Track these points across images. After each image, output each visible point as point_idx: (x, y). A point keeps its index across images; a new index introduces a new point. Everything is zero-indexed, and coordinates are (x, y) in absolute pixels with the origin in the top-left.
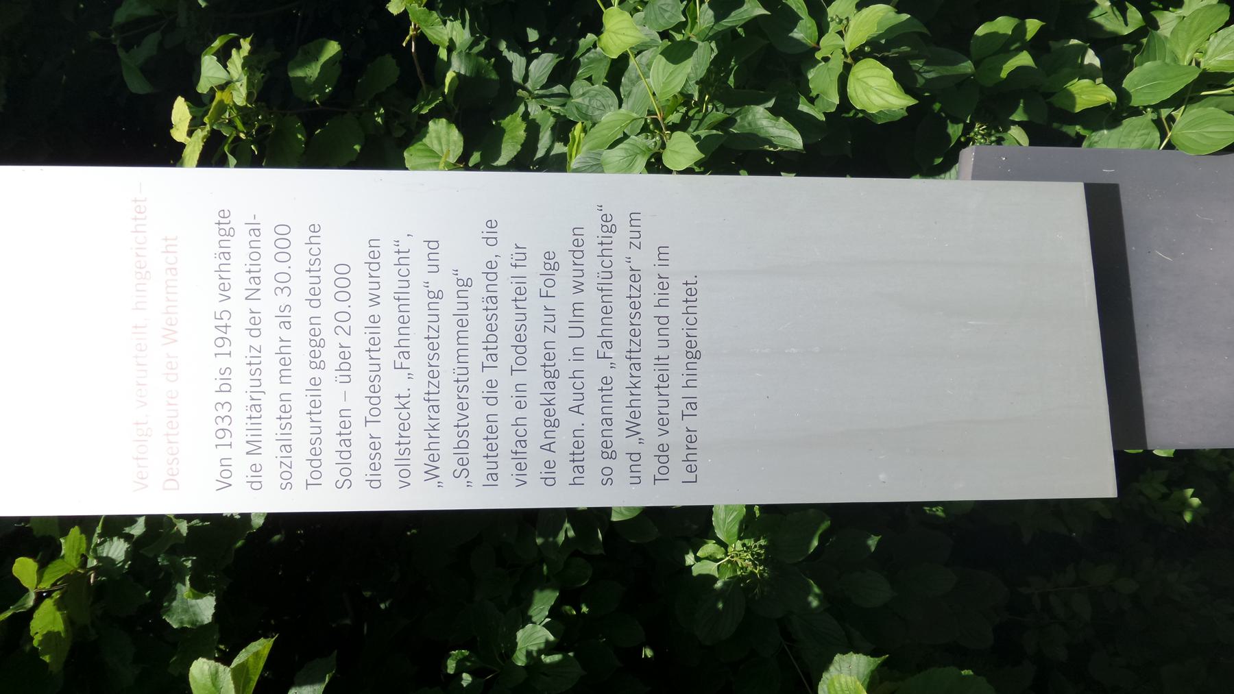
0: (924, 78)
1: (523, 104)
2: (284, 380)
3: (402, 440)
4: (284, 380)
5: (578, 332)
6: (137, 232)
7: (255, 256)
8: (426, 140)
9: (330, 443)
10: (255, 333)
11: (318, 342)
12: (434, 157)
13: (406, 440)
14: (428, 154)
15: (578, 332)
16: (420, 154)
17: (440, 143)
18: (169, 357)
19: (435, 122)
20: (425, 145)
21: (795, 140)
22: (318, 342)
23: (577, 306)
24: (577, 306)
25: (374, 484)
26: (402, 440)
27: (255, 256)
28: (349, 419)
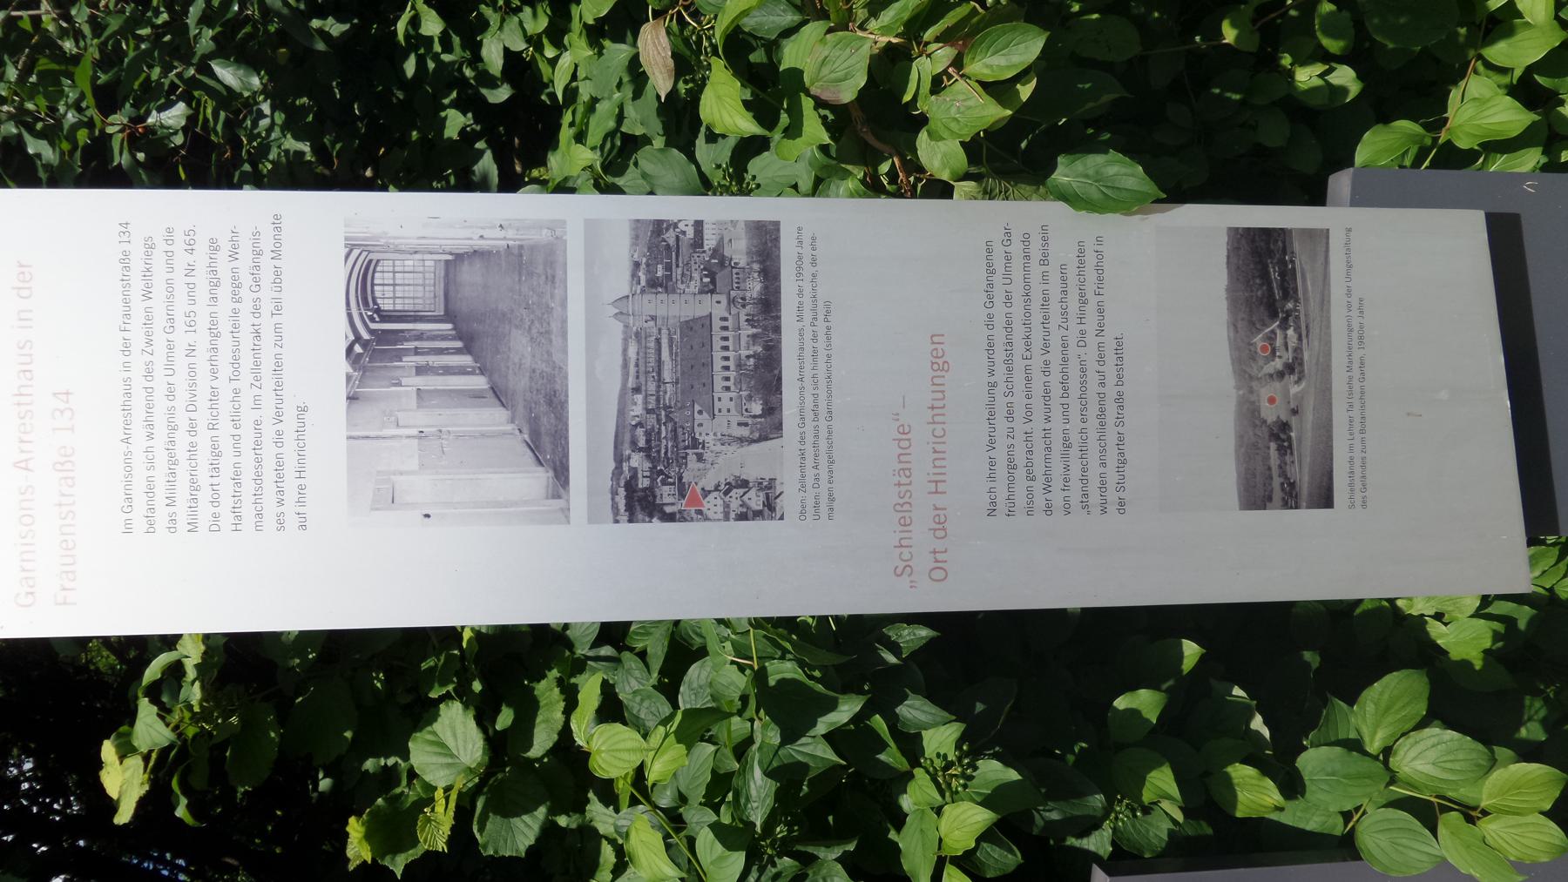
0: (1043, 818)
1: (604, 843)
2: (258, 528)
3: (125, 278)
4: (258, 528)
5: (171, 372)
6: (934, 423)
7: (1027, 315)
8: (436, 726)
9: (269, 476)
10: (1010, 419)
11: (941, 366)
12: (445, 755)
13: (258, 347)
14: (439, 750)
15: (171, 372)
16: (429, 748)
17: (455, 735)
18: (936, 509)
19: (447, 705)
20: (434, 733)
21: (954, 789)
22: (941, 366)
23: (257, 398)
24: (257, 398)
25: (255, 315)
26: (125, 278)
27: (1027, 315)
28: (944, 512)
